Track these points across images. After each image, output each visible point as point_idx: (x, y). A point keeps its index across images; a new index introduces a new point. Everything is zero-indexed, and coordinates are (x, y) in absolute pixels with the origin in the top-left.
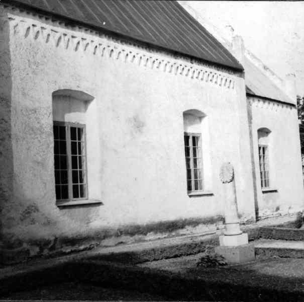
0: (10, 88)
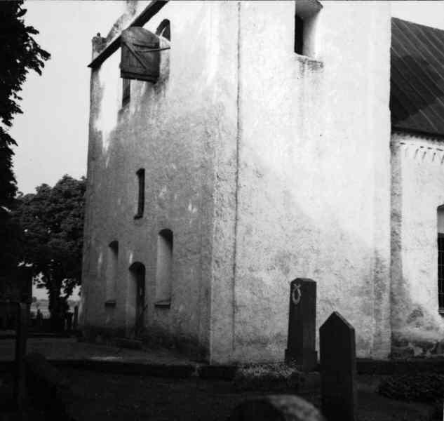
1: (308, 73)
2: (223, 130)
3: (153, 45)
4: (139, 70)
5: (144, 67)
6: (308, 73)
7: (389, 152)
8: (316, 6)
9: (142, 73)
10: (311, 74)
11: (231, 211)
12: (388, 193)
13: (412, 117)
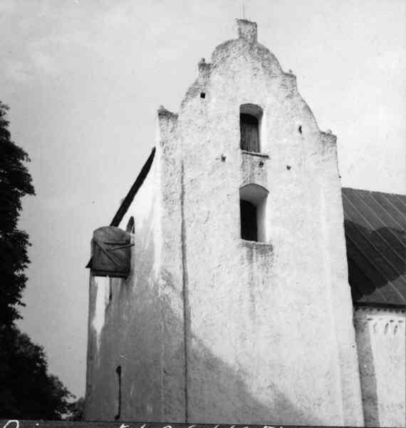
0: (376, 388)
1: (257, 257)
2: (168, 323)
3: (125, 242)
4: (110, 268)
5: (116, 265)
6: (257, 257)
7: (353, 329)
8: (264, 192)
9: (113, 270)
10: (260, 258)
11: (179, 408)
12: (357, 374)
13: (378, 291)
